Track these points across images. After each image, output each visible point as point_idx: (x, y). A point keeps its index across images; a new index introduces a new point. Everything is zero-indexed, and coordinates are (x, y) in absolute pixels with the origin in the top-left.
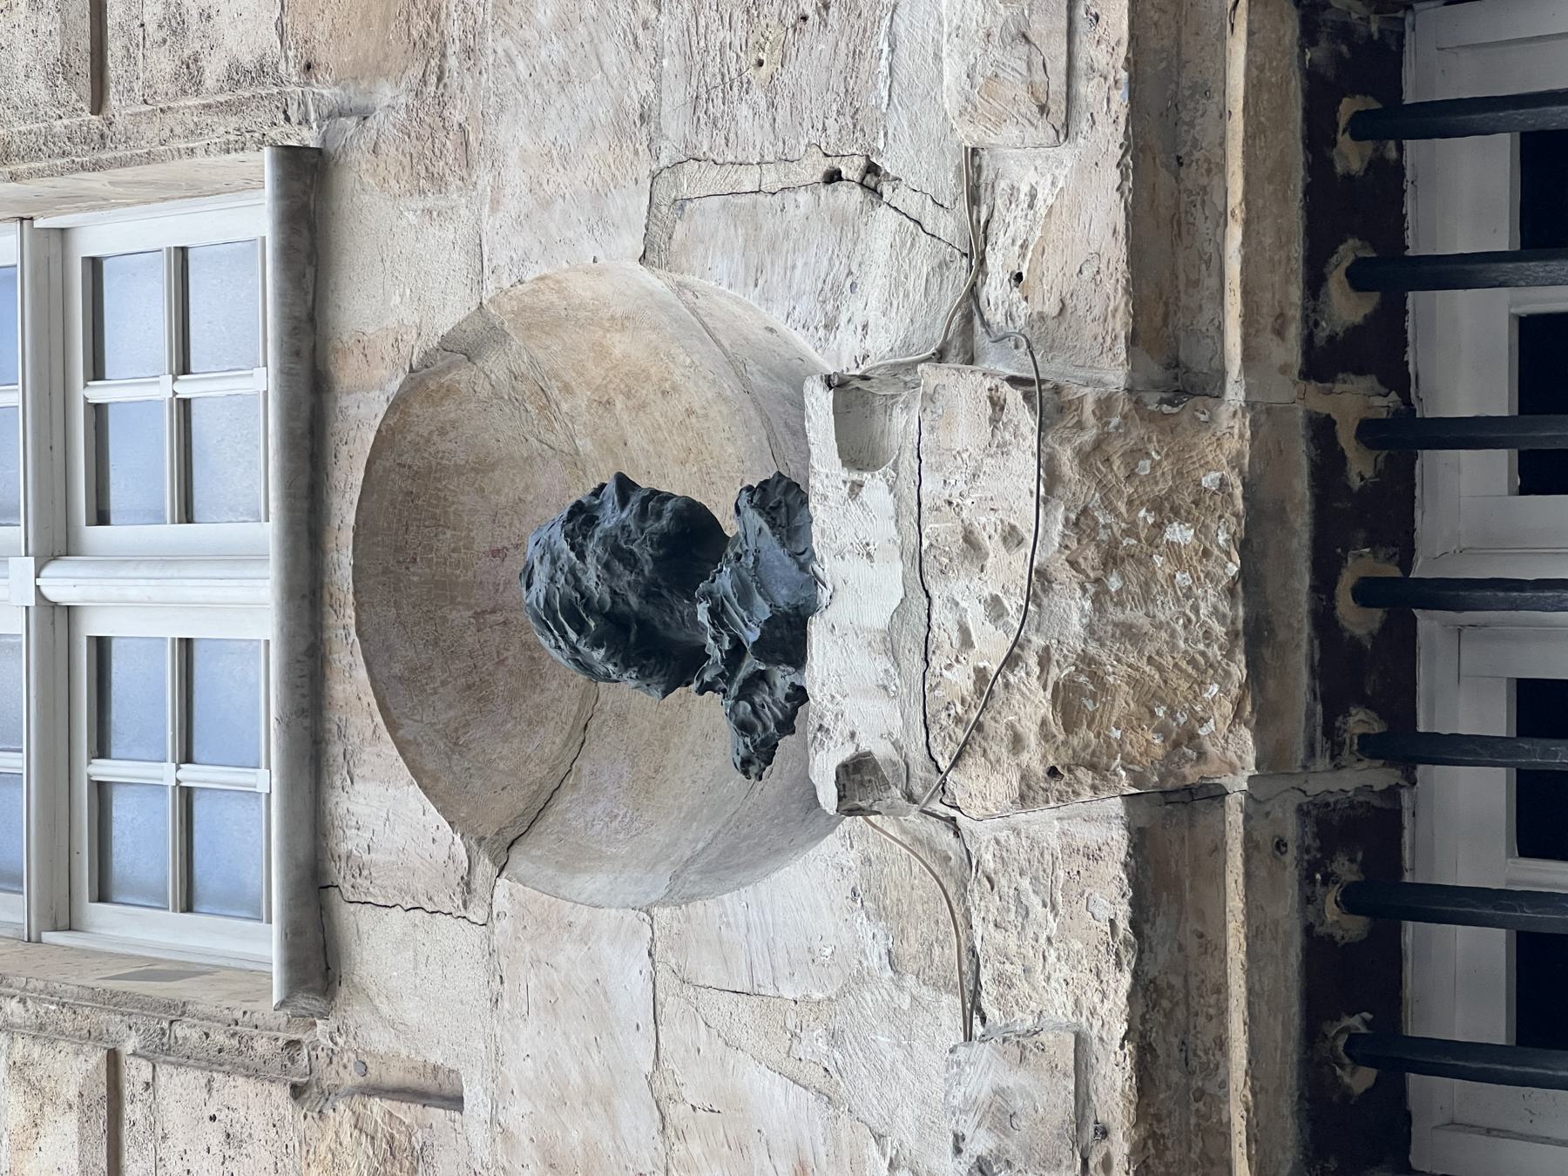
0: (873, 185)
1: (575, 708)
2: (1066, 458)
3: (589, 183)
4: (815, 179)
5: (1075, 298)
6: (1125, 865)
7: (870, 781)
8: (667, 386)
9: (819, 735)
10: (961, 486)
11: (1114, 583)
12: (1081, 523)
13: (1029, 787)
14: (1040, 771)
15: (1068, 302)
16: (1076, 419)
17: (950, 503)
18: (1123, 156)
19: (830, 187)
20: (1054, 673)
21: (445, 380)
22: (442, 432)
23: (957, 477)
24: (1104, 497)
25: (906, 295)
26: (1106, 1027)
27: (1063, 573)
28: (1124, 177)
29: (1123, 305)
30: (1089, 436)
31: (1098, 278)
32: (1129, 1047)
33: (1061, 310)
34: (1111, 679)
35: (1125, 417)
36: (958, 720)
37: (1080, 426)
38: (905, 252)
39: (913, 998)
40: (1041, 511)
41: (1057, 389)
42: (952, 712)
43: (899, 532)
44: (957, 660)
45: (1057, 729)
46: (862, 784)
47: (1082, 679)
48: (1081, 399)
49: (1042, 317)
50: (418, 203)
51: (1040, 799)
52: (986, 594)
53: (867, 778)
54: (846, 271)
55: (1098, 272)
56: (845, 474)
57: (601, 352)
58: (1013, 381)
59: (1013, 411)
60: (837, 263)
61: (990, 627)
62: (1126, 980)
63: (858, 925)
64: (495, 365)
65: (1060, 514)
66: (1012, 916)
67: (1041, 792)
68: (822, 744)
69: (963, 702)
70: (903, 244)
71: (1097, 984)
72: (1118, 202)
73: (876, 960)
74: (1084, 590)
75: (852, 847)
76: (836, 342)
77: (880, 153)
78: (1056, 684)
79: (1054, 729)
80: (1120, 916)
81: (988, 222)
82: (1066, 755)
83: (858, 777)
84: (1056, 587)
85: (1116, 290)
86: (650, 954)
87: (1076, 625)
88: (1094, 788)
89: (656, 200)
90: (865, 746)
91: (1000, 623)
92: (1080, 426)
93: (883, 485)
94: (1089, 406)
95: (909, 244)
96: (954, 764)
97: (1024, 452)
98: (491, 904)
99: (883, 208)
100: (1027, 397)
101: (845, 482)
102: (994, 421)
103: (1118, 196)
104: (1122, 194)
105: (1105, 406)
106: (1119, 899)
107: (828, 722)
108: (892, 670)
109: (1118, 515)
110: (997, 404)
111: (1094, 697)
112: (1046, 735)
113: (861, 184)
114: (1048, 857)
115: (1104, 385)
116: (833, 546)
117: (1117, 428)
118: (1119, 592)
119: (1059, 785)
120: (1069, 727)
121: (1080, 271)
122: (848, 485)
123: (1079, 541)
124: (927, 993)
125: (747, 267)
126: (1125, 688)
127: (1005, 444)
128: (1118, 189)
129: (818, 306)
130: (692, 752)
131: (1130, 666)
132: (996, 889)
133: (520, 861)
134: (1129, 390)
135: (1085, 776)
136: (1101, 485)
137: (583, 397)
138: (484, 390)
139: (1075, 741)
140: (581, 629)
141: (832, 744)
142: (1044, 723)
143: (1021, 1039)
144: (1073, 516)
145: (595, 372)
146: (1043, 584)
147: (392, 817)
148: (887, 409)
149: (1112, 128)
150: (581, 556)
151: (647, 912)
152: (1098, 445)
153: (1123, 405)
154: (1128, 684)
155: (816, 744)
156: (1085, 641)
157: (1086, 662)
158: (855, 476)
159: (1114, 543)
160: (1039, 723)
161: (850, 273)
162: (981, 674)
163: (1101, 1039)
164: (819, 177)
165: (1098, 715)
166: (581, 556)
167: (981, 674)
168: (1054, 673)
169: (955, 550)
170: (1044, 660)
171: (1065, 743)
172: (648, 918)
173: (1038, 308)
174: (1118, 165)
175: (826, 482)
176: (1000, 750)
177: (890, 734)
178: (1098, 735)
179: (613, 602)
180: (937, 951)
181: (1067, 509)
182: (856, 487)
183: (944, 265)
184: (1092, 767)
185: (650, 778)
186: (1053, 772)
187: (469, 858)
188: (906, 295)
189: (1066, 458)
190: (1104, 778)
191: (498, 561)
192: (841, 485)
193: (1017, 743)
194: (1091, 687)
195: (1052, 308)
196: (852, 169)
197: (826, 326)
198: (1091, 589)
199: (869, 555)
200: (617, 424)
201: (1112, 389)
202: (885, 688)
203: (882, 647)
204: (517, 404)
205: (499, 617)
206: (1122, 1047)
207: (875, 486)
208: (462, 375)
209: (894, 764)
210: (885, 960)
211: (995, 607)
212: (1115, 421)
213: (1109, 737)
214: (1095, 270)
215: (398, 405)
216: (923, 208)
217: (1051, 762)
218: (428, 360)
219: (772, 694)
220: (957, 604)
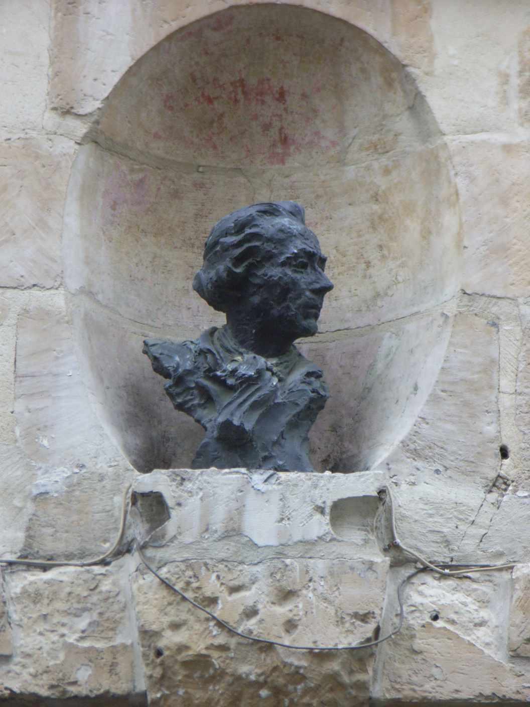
0: (497, 484)
1: (180, 160)
2: (334, 666)
3: (515, 241)
4: (504, 438)
5: (423, 662)
6: (107, 692)
7: (152, 510)
8: (385, 252)
9: (179, 478)
10: (320, 590)
11: (264, 693)
12: (297, 676)
13: (151, 637)
14: (161, 644)
15: (419, 657)
16: (355, 669)
17: (310, 580)
18: (499, 697)
19: (498, 451)
20: (215, 654)
21: (397, 85)
22: (363, 70)
23: (326, 587)
24: (311, 689)
25: (431, 516)
26: (16, 676)
27: (270, 661)
28: (487, 697)
29: (417, 696)
30: (346, 679)
31: (432, 679)
32: (7, 692)
33: (416, 652)
34: (211, 687)
35: (355, 697)
36: (188, 583)
37: (351, 672)
38: (455, 513)
39: (21, 509)
40: (305, 650)
41: (372, 655)
42: (192, 580)
43: (296, 543)
44: (222, 584)
45: (183, 656)
46: (151, 505)
47: (211, 671)
48: (366, 671)
49: (412, 637)
50: (515, 68)
51: (145, 643)
52: (260, 606)
53: (154, 508)
54: (448, 466)
55: (436, 679)
56: (329, 503)
57: (409, 208)
58: (377, 631)
59: (361, 630)
60: (452, 458)
61: (241, 609)
62: (44, 692)
63: (62, 468)
64: (403, 123)
65: (304, 663)
66: (76, 606)
67: (148, 643)
68: (174, 480)
69: (199, 588)
70: (461, 512)
71: (40, 671)
72: (474, 693)
73: (42, 482)
74: (262, 674)
75: (111, 466)
76: (405, 459)
77: (515, 491)
78: (208, 656)
79: (184, 654)
80: (80, 689)
81: (469, 578)
82: (169, 662)
83: (154, 503)
84: (263, 656)
85: (425, 691)
86: (34, 285)
87: (244, 669)
88: (151, 677)
89: (500, 302)
90: (173, 513)
91: (243, 616)
92: (351, 672)
93: (321, 533)
94: (361, 677)
95: (461, 517)
96: (163, 581)
97: (338, 638)
98: (55, 133)
99: (482, 495)
100: (368, 640)
101: (324, 502)
102: (356, 615)
103: (477, 694)
104: (477, 697)
105: (362, 686)
106: (89, 688)
107: (189, 485)
108: (216, 535)
109: (302, 697)
110: (365, 618)
111: (202, 677)
112: (182, 648)
113: (499, 476)
114: (110, 634)
115: (373, 683)
116: (288, 493)
117: (350, 693)
118: (259, 696)
119: (152, 655)
120: (185, 664)
121: (437, 667)
122: (322, 505)
123: (288, 674)
124: (24, 520)
125: (453, 383)
126: (207, 696)
127: (343, 623)
128: (480, 693)
129: (428, 444)
130: (155, 257)
131: (219, 701)
132: (91, 592)
133: (88, 147)
134: (370, 698)
135: (158, 672)
136: (318, 688)
137: (382, 182)
138: (389, 108)
139: (177, 667)
140: (238, 261)
141: (174, 488)
142: (187, 648)
143: (6, 614)
144: (302, 671)
145: (397, 199)
146: (264, 647)
147: (109, 37)
148: (364, 527)
149: (514, 689)
150: (283, 264)
151: (61, 284)
152: (342, 686)
153: (362, 696)
154: (208, 699)
155: (174, 476)
156: (232, 675)
157: (221, 674)
158: (328, 510)
159: (287, 694)
160: (188, 644)
161: (446, 469)
162: (213, 601)
163: (9, 672)
164: (505, 442)
165: (191, 680)
166: (283, 264)
167: (213, 601)
168: (215, 654)
169: (284, 583)
170: (223, 648)
171: (176, 661)
172: (57, 284)
173: (418, 635)
174: (494, 694)
175: (325, 488)
176: (173, 615)
177: (180, 534)
178: (180, 681)
179: (255, 285)
180: (50, 531)
181: (305, 668)
182: (321, 510)
183: (447, 543)
184: (163, 677)
185: (139, 227)
186: (159, 653)
187: (86, 115)
188: (431, 516)
189: (334, 666)
190: (156, 683)
191: (277, 96)
192: (323, 500)
193: (176, 626)
194: (207, 676)
195: (418, 644)
196: (507, 467)
197: (415, 450)
198: (262, 679)
199: (282, 519)
200: (362, 202)
201: (371, 689)
202: (207, 530)
203: (229, 529)
204: (379, 129)
205: (240, 96)
206: (6, 689)
207: (320, 525)
208: (399, 97)
209: (163, 536)
210: (42, 490)
211: (251, 612)
212: (354, 692)
213: (179, 687)
214: (437, 677)
215: (380, 49)
216: (481, 527)
217: (166, 653)
218: (410, 79)
219: (199, 405)
220: (253, 583)
